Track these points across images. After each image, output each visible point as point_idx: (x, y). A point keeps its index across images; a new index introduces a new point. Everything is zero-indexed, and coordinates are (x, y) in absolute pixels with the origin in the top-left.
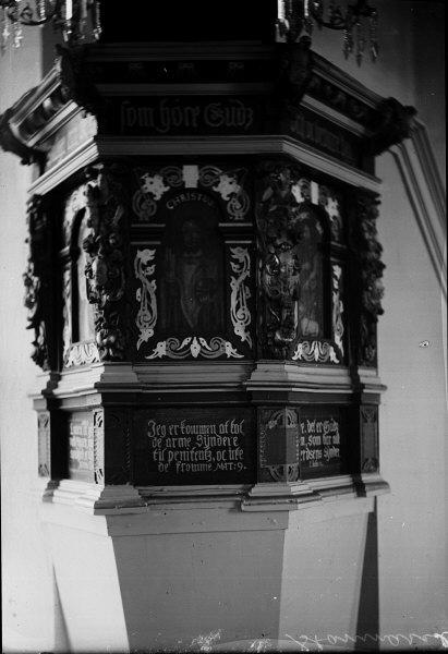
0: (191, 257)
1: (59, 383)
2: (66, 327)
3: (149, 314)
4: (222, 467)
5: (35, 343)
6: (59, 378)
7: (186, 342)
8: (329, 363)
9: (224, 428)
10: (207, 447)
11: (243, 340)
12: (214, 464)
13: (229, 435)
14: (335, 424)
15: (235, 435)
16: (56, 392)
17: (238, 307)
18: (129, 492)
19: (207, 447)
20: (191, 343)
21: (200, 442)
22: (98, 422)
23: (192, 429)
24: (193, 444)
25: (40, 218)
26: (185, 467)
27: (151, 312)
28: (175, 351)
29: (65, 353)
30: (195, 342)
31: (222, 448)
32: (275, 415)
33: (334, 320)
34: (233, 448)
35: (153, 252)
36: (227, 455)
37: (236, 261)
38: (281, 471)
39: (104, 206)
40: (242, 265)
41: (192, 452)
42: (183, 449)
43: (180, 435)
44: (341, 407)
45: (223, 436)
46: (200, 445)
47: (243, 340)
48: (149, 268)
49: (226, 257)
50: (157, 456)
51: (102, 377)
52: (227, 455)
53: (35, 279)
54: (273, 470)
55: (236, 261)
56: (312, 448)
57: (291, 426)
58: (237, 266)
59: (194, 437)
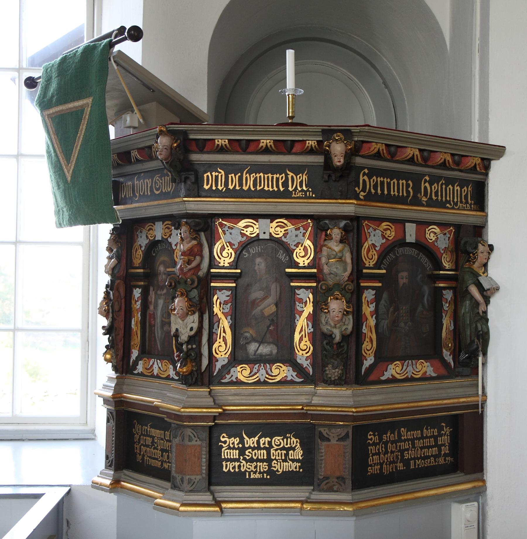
14: (293, 439)
21: (156, 443)
24: (153, 442)
57: (194, 443)
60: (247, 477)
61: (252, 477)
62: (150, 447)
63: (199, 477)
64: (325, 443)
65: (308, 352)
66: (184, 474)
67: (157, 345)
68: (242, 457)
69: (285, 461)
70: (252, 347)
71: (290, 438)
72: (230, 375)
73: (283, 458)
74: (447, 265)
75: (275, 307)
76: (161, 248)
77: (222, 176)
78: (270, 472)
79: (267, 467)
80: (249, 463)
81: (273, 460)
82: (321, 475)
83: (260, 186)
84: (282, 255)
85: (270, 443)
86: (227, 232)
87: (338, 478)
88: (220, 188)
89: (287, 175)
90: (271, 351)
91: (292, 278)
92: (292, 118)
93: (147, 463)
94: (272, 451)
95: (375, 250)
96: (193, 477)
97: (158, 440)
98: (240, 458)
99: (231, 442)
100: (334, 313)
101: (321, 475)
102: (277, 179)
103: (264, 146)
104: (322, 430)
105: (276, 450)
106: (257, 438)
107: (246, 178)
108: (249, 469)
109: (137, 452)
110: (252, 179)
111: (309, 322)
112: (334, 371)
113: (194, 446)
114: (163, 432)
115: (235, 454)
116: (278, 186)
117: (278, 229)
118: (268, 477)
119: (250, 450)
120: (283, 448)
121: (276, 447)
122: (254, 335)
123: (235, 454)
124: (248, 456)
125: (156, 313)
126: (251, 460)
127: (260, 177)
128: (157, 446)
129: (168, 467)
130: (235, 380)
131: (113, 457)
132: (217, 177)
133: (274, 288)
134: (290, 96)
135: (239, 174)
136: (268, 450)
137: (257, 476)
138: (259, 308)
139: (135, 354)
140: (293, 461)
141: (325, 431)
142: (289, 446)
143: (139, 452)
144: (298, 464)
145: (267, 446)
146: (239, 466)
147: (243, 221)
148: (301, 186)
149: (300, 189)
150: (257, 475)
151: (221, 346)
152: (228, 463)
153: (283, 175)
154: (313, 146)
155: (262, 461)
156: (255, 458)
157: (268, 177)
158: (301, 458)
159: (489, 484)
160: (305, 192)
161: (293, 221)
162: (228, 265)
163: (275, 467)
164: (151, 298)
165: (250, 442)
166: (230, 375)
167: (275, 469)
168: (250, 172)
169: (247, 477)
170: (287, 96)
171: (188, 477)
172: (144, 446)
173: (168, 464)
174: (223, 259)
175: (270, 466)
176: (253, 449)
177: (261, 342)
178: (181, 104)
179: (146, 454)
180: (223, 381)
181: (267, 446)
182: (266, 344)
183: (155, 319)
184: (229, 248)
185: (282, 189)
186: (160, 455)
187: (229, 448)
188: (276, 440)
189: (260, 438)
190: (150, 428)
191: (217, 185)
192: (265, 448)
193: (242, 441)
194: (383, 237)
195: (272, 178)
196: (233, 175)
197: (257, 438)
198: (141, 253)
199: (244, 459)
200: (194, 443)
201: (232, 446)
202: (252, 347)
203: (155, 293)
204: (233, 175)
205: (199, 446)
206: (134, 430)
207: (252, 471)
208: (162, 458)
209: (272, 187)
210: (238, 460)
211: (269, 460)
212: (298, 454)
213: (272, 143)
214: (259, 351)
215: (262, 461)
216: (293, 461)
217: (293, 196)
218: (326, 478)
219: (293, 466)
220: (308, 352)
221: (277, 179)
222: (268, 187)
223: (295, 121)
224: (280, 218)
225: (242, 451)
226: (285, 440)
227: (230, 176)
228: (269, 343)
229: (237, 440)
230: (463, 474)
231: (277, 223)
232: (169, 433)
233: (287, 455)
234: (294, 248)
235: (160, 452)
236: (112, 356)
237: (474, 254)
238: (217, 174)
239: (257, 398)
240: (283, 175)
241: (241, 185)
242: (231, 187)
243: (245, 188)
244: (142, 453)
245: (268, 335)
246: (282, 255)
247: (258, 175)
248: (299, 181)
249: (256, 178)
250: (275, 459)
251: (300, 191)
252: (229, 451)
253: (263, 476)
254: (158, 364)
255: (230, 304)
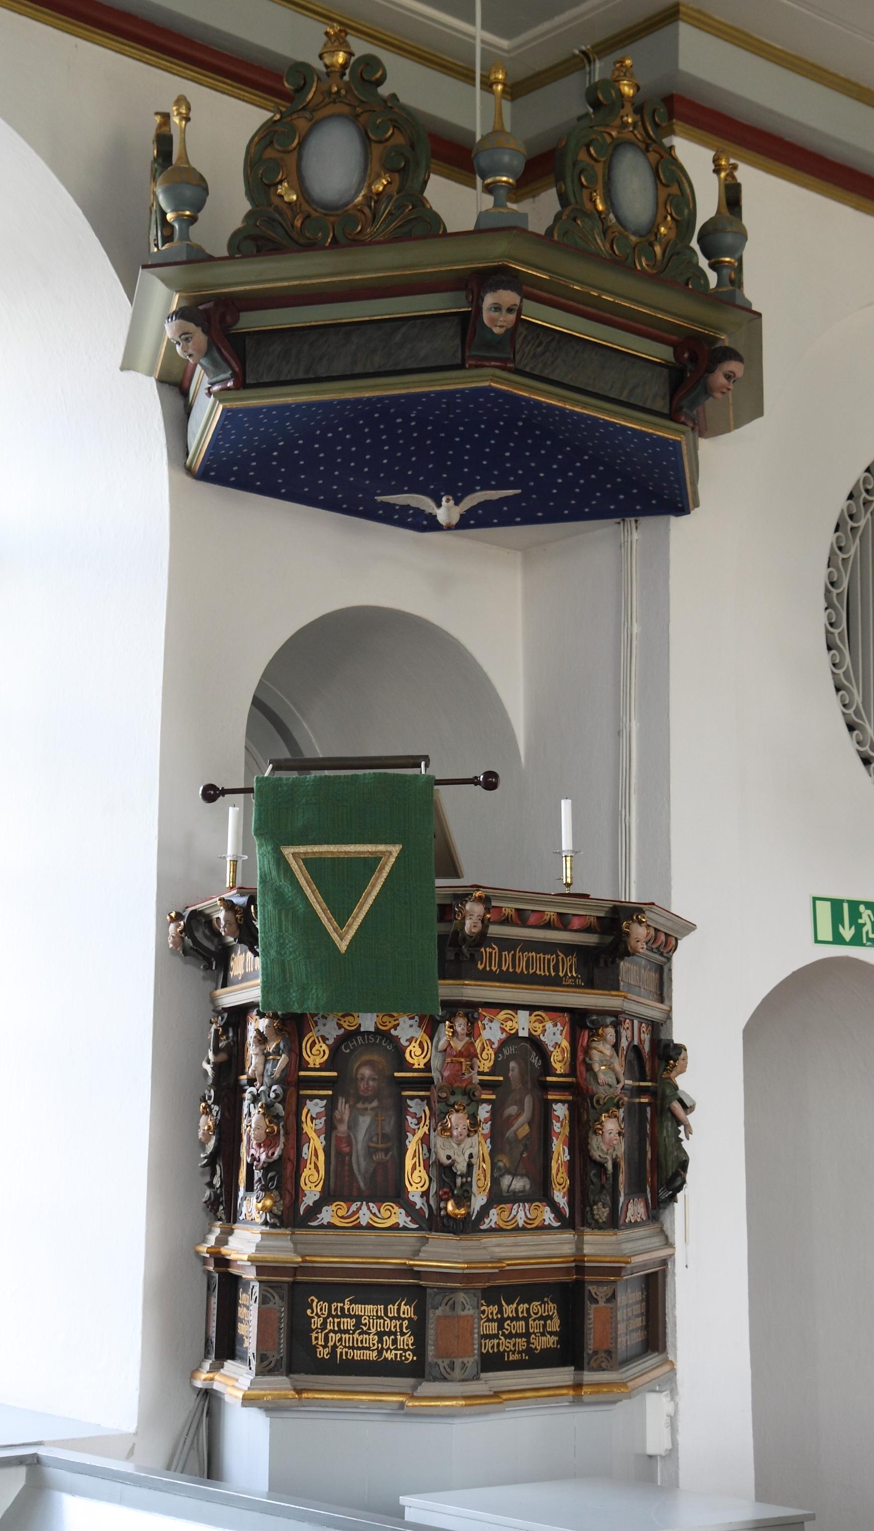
0: (366, 1109)
1: (230, 1238)
2: (242, 1168)
3: (316, 1173)
4: (389, 1355)
5: (210, 1185)
6: (231, 1232)
7: (354, 1207)
8: (544, 1228)
9: (392, 1309)
10: (373, 1331)
11: (417, 1207)
12: (380, 1352)
13: (399, 1318)
14: (551, 1305)
15: (404, 1319)
16: (224, 1250)
17: (414, 1168)
18: (280, 1385)
19: (373, 1331)
20: (359, 1209)
21: (365, 1325)
22: (254, 1298)
23: (358, 1309)
24: (358, 1325)
25: (225, 1032)
26: (346, 1353)
27: (318, 1171)
28: (342, 1217)
29: (239, 1201)
30: (364, 1207)
31: (390, 1333)
32: (447, 1299)
33: (554, 1171)
34: (403, 1334)
35: (325, 1102)
36: (395, 1342)
37: (414, 1115)
38: (452, 1366)
39: (269, 1054)
40: (419, 1120)
41: (356, 1336)
42: (347, 1332)
43: (343, 1315)
44: (563, 1285)
45: (391, 1319)
46: (365, 1329)
47: (417, 1207)
48: (318, 1121)
49: (401, 1110)
50: (317, 1338)
51: (258, 1248)
52: (395, 1342)
53: (216, 1108)
54: (443, 1363)
55: (414, 1115)
56: (510, 1336)
57: (466, 1312)
58: (415, 1121)
59: (358, 1318)
60: (506, 1359)
61: (511, 1358)
62: (351, 1332)
63: (471, 1359)
64: (594, 1306)
65: (564, 1187)
66: (455, 1357)
67: (357, 1182)
68: (500, 1332)
69: (543, 1334)
70: (506, 1181)
71: (547, 1302)
72: (489, 1219)
73: (541, 1331)
74: (559, 1067)
75: (528, 1127)
76: (364, 1041)
77: (495, 953)
78: (529, 1351)
79: (525, 1344)
80: (508, 1340)
81: (532, 1334)
82: (590, 1349)
83: (532, 969)
84: (535, 1057)
85: (528, 1310)
86: (486, 1026)
87: (605, 1352)
88: (494, 969)
89: (557, 956)
90: (524, 1187)
91: (402, 1086)
92: (568, 885)
93: (344, 1357)
94: (531, 1322)
95: (491, 1047)
96: (466, 1360)
97: (371, 1321)
98: (499, 1333)
99: (490, 1312)
100: (612, 1135)
101: (590, 1349)
102: (549, 960)
103: (548, 920)
104: (590, 1288)
105: (534, 1320)
106: (515, 1305)
107: (519, 957)
108: (508, 1347)
109: (317, 1344)
110: (525, 959)
111: (565, 1147)
112: (603, 1210)
113: (467, 1316)
114: (382, 1307)
115: (493, 1328)
116: (549, 971)
117: (537, 1024)
118: (527, 1358)
119: (509, 1322)
120: (541, 1318)
121: (534, 1316)
122: (508, 1165)
123: (493, 1328)
124: (507, 1330)
125: (354, 1135)
126: (510, 1336)
127: (532, 956)
128: (369, 1329)
129: (393, 1357)
130: (493, 1226)
131: (282, 1355)
132: (491, 953)
133: (528, 1101)
134: (568, 859)
135: (513, 952)
136: (526, 1319)
137: (516, 1357)
138: (513, 1128)
139: (622, 1199)
140: (551, 1333)
141: (592, 1289)
142: (546, 1313)
143: (323, 1344)
144: (556, 1338)
145: (525, 1315)
146: (498, 1344)
147: (503, 1012)
148: (571, 972)
149: (570, 975)
150: (516, 1355)
151: (479, 1179)
152: (487, 1341)
153: (554, 956)
154: (552, 920)
155: (520, 1336)
156: (514, 1332)
157: (540, 957)
158: (558, 1330)
159: (680, 1367)
160: (575, 978)
161: (553, 1014)
162: (488, 1070)
163: (533, 1344)
164: (342, 1114)
165: (509, 1310)
166: (489, 1219)
167: (533, 1347)
168: (523, 951)
169: (506, 1359)
170: (564, 858)
171: (461, 1360)
172: (335, 1332)
173: (393, 1352)
174: (483, 1062)
175: (528, 1342)
176: (512, 1319)
177: (514, 1175)
178: (242, 817)
179: (341, 1344)
180: (482, 1227)
181: (525, 1315)
182: (519, 1177)
183: (352, 1144)
184: (489, 1048)
185: (553, 974)
186: (375, 1342)
187: (488, 1320)
188: (535, 1307)
189: (518, 1304)
190: (351, 1304)
191: (490, 966)
192: (523, 1318)
193: (500, 1311)
194: (503, 1030)
195: (544, 958)
196: (506, 953)
197: (515, 1305)
198: (491, 1052)
199: (503, 1334)
200: (466, 1312)
201: (490, 1317)
202: (506, 1181)
203: (350, 1107)
204: (506, 953)
205: (472, 1316)
206: (309, 1312)
207: (511, 1350)
208: (380, 1345)
209: (544, 972)
210: (495, 1336)
211: (527, 1335)
212: (554, 1325)
213: (555, 917)
214: (512, 1187)
215: (520, 1336)
216: (551, 1333)
217: (564, 983)
218: (596, 1353)
219: (550, 1341)
220: (564, 1187)
221: (549, 960)
222: (540, 970)
223: (573, 890)
224: (538, 1010)
225: (501, 1322)
226: (543, 1306)
227: (503, 953)
228: (522, 1176)
229: (495, 1309)
230: (656, 1354)
231: (536, 1016)
232: (396, 1307)
233: (545, 1326)
234: (408, 1043)
235: (376, 1337)
236: (275, 1202)
237: (675, 1061)
238: (491, 950)
239: (523, 1248)
240: (554, 956)
241: (514, 967)
242: (504, 968)
243: (518, 971)
244: (331, 1344)
245: (521, 1165)
246: (535, 1057)
247: (530, 954)
248: (569, 964)
249: (529, 958)
250: (534, 1333)
251: (570, 978)
252: (487, 1324)
253: (522, 1356)
254: (371, 1208)
255: (490, 1123)
